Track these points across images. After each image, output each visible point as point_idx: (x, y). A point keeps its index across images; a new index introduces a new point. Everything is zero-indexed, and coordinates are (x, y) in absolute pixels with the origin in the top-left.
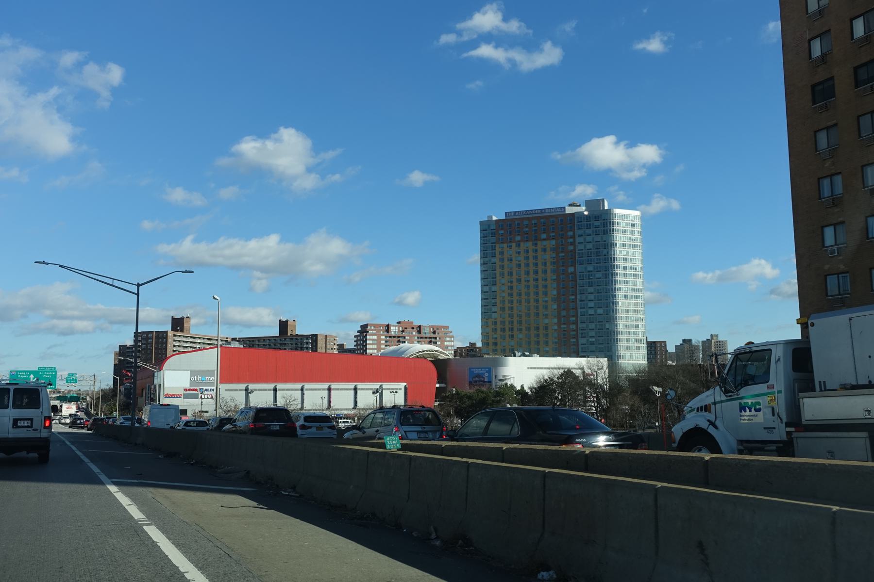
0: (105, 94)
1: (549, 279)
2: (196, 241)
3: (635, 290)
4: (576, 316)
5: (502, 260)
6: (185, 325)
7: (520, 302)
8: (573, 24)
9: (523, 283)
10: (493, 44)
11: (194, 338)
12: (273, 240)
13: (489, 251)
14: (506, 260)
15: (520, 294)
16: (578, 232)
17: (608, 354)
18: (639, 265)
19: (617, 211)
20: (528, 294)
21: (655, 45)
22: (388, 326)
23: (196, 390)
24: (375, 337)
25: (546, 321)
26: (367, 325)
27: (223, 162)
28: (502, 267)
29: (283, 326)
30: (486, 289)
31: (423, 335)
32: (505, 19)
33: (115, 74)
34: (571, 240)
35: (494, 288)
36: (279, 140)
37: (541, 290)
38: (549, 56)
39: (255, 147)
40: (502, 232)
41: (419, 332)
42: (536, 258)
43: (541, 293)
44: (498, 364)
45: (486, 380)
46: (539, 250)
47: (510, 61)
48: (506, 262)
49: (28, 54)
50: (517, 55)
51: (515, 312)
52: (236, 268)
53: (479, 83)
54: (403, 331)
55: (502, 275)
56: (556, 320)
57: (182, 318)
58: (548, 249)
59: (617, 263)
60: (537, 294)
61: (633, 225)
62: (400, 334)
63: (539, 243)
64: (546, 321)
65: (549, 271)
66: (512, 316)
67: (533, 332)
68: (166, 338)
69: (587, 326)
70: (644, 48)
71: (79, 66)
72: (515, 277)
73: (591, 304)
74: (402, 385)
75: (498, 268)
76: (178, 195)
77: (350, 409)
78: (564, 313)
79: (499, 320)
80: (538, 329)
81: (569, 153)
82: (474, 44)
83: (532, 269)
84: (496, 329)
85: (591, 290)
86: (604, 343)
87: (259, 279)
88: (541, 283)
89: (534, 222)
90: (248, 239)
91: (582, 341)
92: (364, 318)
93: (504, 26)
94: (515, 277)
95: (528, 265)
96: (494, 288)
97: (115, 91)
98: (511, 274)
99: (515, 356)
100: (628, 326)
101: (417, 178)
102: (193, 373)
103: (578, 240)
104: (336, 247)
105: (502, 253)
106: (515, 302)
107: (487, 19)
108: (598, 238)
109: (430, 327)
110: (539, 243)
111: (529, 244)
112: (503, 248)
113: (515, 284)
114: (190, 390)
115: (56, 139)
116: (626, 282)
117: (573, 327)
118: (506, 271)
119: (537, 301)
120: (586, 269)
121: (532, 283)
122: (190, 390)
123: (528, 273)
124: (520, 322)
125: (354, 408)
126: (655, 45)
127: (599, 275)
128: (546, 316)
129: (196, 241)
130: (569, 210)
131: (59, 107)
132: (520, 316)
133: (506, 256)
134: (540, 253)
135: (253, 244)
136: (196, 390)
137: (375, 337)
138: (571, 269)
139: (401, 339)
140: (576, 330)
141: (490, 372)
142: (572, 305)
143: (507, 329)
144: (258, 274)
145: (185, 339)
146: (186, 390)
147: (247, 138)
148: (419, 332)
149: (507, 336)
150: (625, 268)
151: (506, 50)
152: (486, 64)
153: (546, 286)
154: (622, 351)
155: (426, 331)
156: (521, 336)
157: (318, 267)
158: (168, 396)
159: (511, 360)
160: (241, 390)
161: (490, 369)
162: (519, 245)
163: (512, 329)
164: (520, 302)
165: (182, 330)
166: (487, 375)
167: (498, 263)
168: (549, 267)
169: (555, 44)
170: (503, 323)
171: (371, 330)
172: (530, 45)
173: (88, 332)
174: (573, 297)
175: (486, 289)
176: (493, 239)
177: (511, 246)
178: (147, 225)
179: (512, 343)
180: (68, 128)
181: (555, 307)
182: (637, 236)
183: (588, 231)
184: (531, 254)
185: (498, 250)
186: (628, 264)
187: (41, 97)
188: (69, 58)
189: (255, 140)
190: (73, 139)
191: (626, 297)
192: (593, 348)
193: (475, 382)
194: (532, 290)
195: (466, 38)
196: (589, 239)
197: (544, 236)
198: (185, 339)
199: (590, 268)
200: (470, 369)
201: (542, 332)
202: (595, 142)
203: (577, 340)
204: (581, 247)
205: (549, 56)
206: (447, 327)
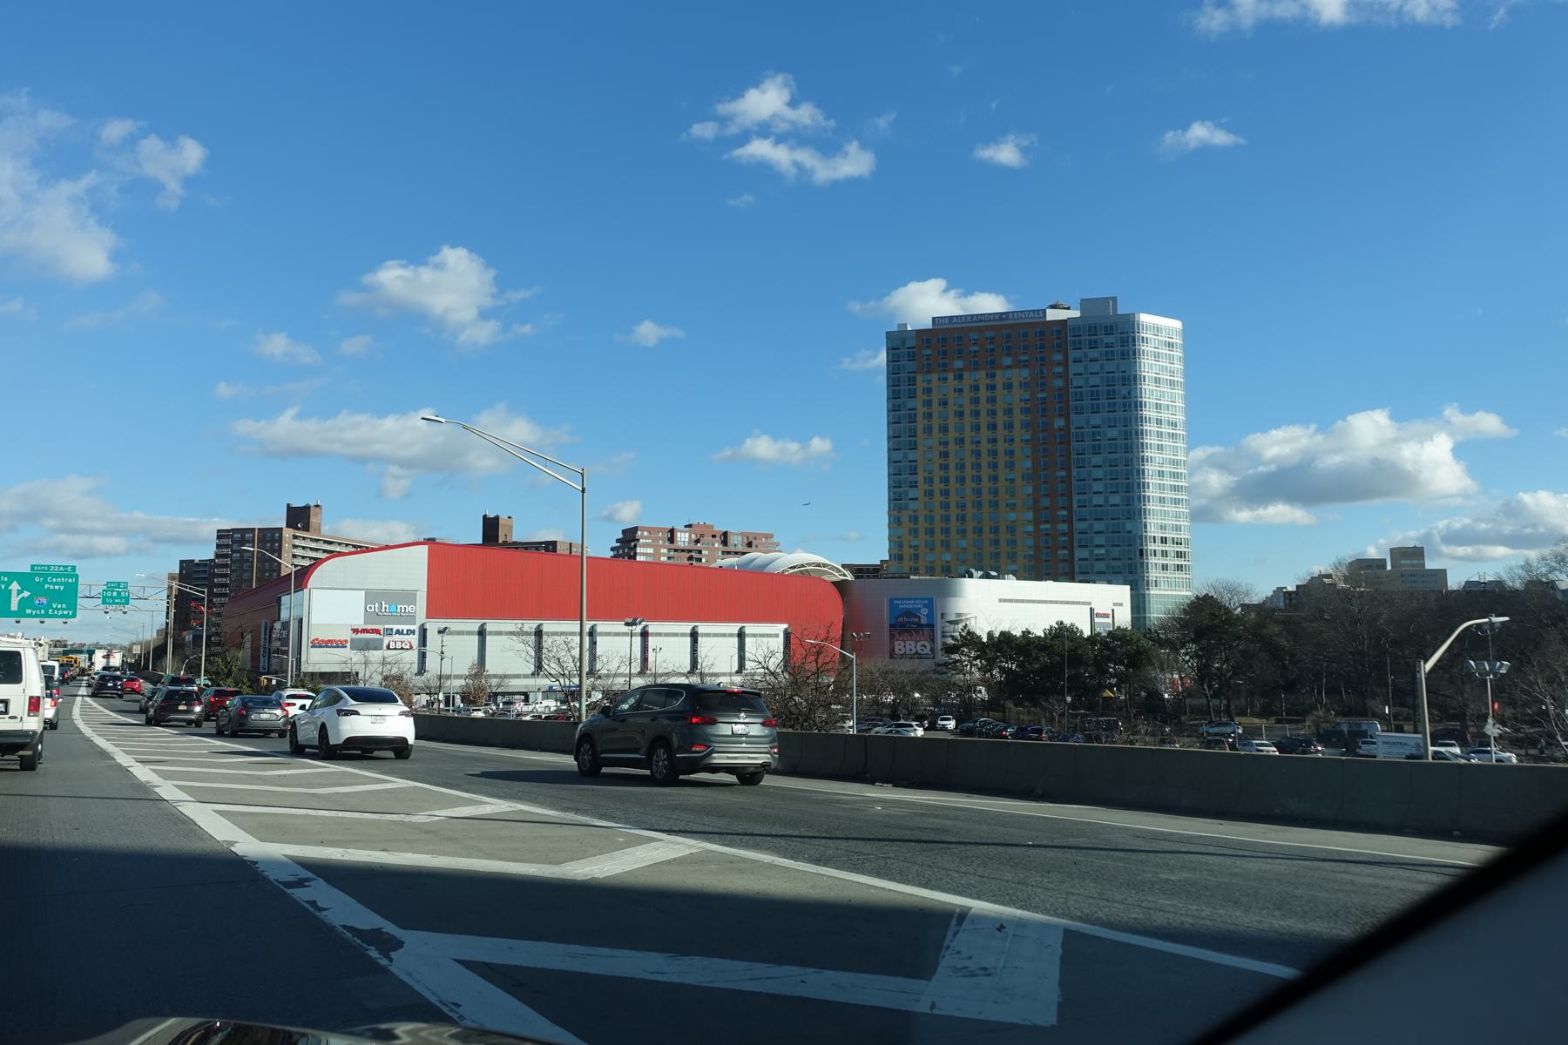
0: (174, 186)
1: (1017, 440)
2: (300, 416)
3: (1175, 463)
4: (1069, 508)
5: (928, 403)
6: (313, 520)
7: (962, 480)
8: (892, 116)
9: (968, 446)
10: (772, 139)
11: (330, 543)
12: (415, 421)
13: (904, 387)
15: (962, 467)
16: (1072, 354)
17: (1131, 577)
18: (1180, 417)
19: (1144, 318)
20: (978, 466)
21: (1006, 154)
22: (672, 531)
23: (377, 631)
24: (650, 550)
25: (1012, 516)
26: (635, 529)
27: (350, 298)
28: (929, 416)
29: (491, 527)
30: (898, 456)
31: (731, 548)
32: (793, 103)
33: (192, 154)
34: (1060, 369)
35: (912, 455)
36: (440, 267)
37: (1002, 459)
38: (855, 163)
39: (400, 277)
41: (725, 542)
42: (993, 400)
43: (1001, 465)
44: (947, 592)
45: (924, 621)
46: (999, 387)
47: (798, 166)
48: (935, 407)
49: (51, 120)
50: (806, 157)
51: (953, 498)
52: (361, 460)
53: (748, 198)
54: (697, 541)
55: (928, 430)
56: (1030, 515)
57: (307, 508)
58: (1016, 385)
59: (1146, 413)
60: (995, 466)
61: (1170, 345)
62: (693, 546)
63: (999, 372)
64: (1012, 516)
65: (1017, 425)
66: (946, 506)
67: (987, 535)
68: (280, 540)
69: (1091, 526)
70: (991, 158)
71: (132, 141)
72: (952, 435)
73: (1098, 487)
74: (780, 628)
75: (920, 417)
76: (277, 345)
77: (526, 676)
78: (1045, 502)
79: (922, 513)
80: (995, 530)
81: (872, 304)
82: (744, 138)
83: (984, 420)
84: (916, 531)
85: (1097, 460)
86: (1122, 560)
87: (397, 477)
88: (1001, 447)
89: (990, 334)
90: (384, 415)
91: (1080, 553)
92: (629, 514)
93: (791, 114)
94: (952, 435)
95: (977, 414)
96: (912, 455)
97: (189, 182)
98: (944, 429)
99: (971, 576)
100: (1163, 527)
101: (648, 332)
102: (372, 596)
103: (1074, 368)
104: (520, 431)
105: (928, 391)
107: (766, 100)
108: (1111, 366)
109: (742, 534)
110: (999, 372)
111: (981, 375)
113: (952, 448)
114: (364, 631)
115: (89, 256)
116: (1160, 448)
117: (1064, 527)
119: (995, 479)
120: (1088, 420)
121: (985, 447)
122: (364, 631)
123: (977, 428)
124: (962, 518)
125: (739, 672)
126: (1006, 154)
127: (1113, 433)
128: (1012, 507)
129: (300, 416)
130: (1052, 315)
131: (96, 208)
132: (963, 507)
133: (936, 398)
134: (1000, 393)
135: (389, 423)
136: (377, 631)
137: (650, 550)
138: (1059, 423)
139: (695, 555)
140: (1070, 534)
141: (930, 605)
142: (1060, 487)
143: (937, 530)
144: (394, 469)
145: (313, 545)
146: (356, 631)
147: (389, 263)
148: (725, 542)
149: (938, 544)
150: (1159, 422)
151: (792, 148)
152: (763, 169)
153: (1011, 453)
154: (1153, 574)
155: (736, 541)
156: (964, 543)
157: (488, 462)
158: (318, 644)
159: (967, 583)
160: (469, 633)
161: (930, 600)
162: (960, 377)
163: (946, 532)
165: (306, 528)
166: (925, 611)
167: (921, 410)
168: (1018, 418)
169: (864, 146)
170: (930, 519)
171: (643, 538)
172: (828, 146)
173: (118, 555)
174: (1063, 473)
175: (898, 456)
176: (912, 365)
178: (224, 390)
179: (947, 557)
180: (107, 238)
181: (1029, 490)
182: (1178, 366)
183: (1093, 354)
184: (983, 393)
186: (1165, 416)
187: (66, 188)
188: (116, 130)
189: (403, 266)
190: (115, 256)
191: (1161, 474)
192: (1101, 566)
193: (903, 625)
194: (985, 460)
195: (733, 130)
196: (1095, 367)
197: (1008, 361)
198: (313, 545)
199: (1096, 420)
200: (891, 601)
201: (1004, 536)
202: (913, 287)
203: (1072, 551)
204: (1077, 381)
205: (855, 163)
206: (771, 536)
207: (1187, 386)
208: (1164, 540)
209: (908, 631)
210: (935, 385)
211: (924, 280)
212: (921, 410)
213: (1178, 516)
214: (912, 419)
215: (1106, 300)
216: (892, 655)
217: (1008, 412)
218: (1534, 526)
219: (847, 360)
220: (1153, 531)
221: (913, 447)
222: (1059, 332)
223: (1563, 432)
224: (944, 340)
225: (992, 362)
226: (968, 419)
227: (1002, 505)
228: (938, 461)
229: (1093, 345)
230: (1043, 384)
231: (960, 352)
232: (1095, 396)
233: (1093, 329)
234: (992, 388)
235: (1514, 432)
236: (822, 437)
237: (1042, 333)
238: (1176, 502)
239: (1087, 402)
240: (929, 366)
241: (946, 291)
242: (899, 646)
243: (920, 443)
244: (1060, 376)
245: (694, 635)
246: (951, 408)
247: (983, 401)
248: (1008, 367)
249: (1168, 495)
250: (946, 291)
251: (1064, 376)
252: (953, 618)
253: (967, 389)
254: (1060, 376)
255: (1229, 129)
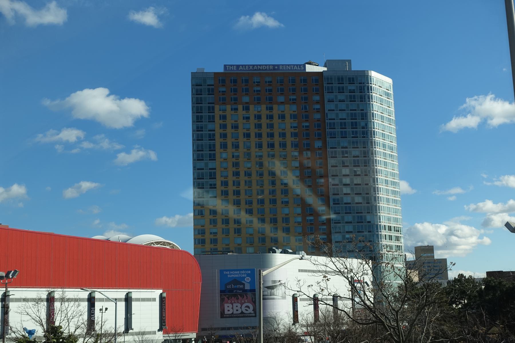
13: (205, 114)
14: (229, 127)
16: (327, 96)
21: (148, 18)
25: (286, 211)
28: (224, 136)
34: (318, 106)
35: (211, 165)
40: (224, 89)
42: (271, 126)
44: (265, 264)
45: (247, 287)
46: (276, 117)
55: (224, 146)
56: (299, 210)
58: (288, 116)
64: (286, 211)
74: (156, 293)
75: (217, 136)
81: (57, 102)
89: (268, 79)
95: (260, 135)
96: (211, 165)
98: (236, 146)
99: (275, 252)
100: (389, 219)
103: (328, 106)
105: (224, 117)
106: (242, 183)
110: (275, 107)
112: (225, 110)
118: (229, 141)
126: (148, 18)
130: (309, 68)
133: (229, 122)
134: (276, 121)
141: (252, 274)
149: (232, 231)
161: (253, 271)
162: (247, 109)
164: (249, 183)
166: (248, 279)
167: (218, 132)
175: (201, 164)
177: (236, 109)
179: (239, 241)
183: (341, 96)
184: (264, 121)
185: (218, 113)
186: (387, 142)
193: (231, 291)
196: (343, 106)
197: (281, 99)
200: (221, 271)
202: (87, 92)
207: (397, 122)
208: (390, 229)
209: (235, 296)
210: (229, 112)
211: (94, 88)
212: (218, 132)
213: (396, 212)
214: (212, 137)
215: (344, 61)
216: (223, 315)
217: (283, 135)
218: (422, 241)
219: (40, 135)
220: (383, 223)
221: (212, 158)
222: (317, 81)
223: (514, 181)
224: (235, 81)
225: (271, 99)
226: (253, 139)
227: (279, 202)
228: (231, 170)
229: (341, 90)
230: (307, 117)
231: (247, 90)
232: (343, 125)
233: (341, 80)
234: (271, 117)
235: (414, 191)
236: (20, 184)
237: (305, 81)
238: (395, 201)
239: (338, 130)
240: (224, 99)
241: (108, 96)
242: (228, 308)
243: (218, 156)
244: (318, 111)
245: (128, 300)
246: (241, 131)
247: (264, 126)
248: (282, 103)
249: (391, 197)
250: (108, 96)
251: (322, 111)
252: (270, 284)
253: (252, 118)
254: (318, 111)
255: (276, 18)
